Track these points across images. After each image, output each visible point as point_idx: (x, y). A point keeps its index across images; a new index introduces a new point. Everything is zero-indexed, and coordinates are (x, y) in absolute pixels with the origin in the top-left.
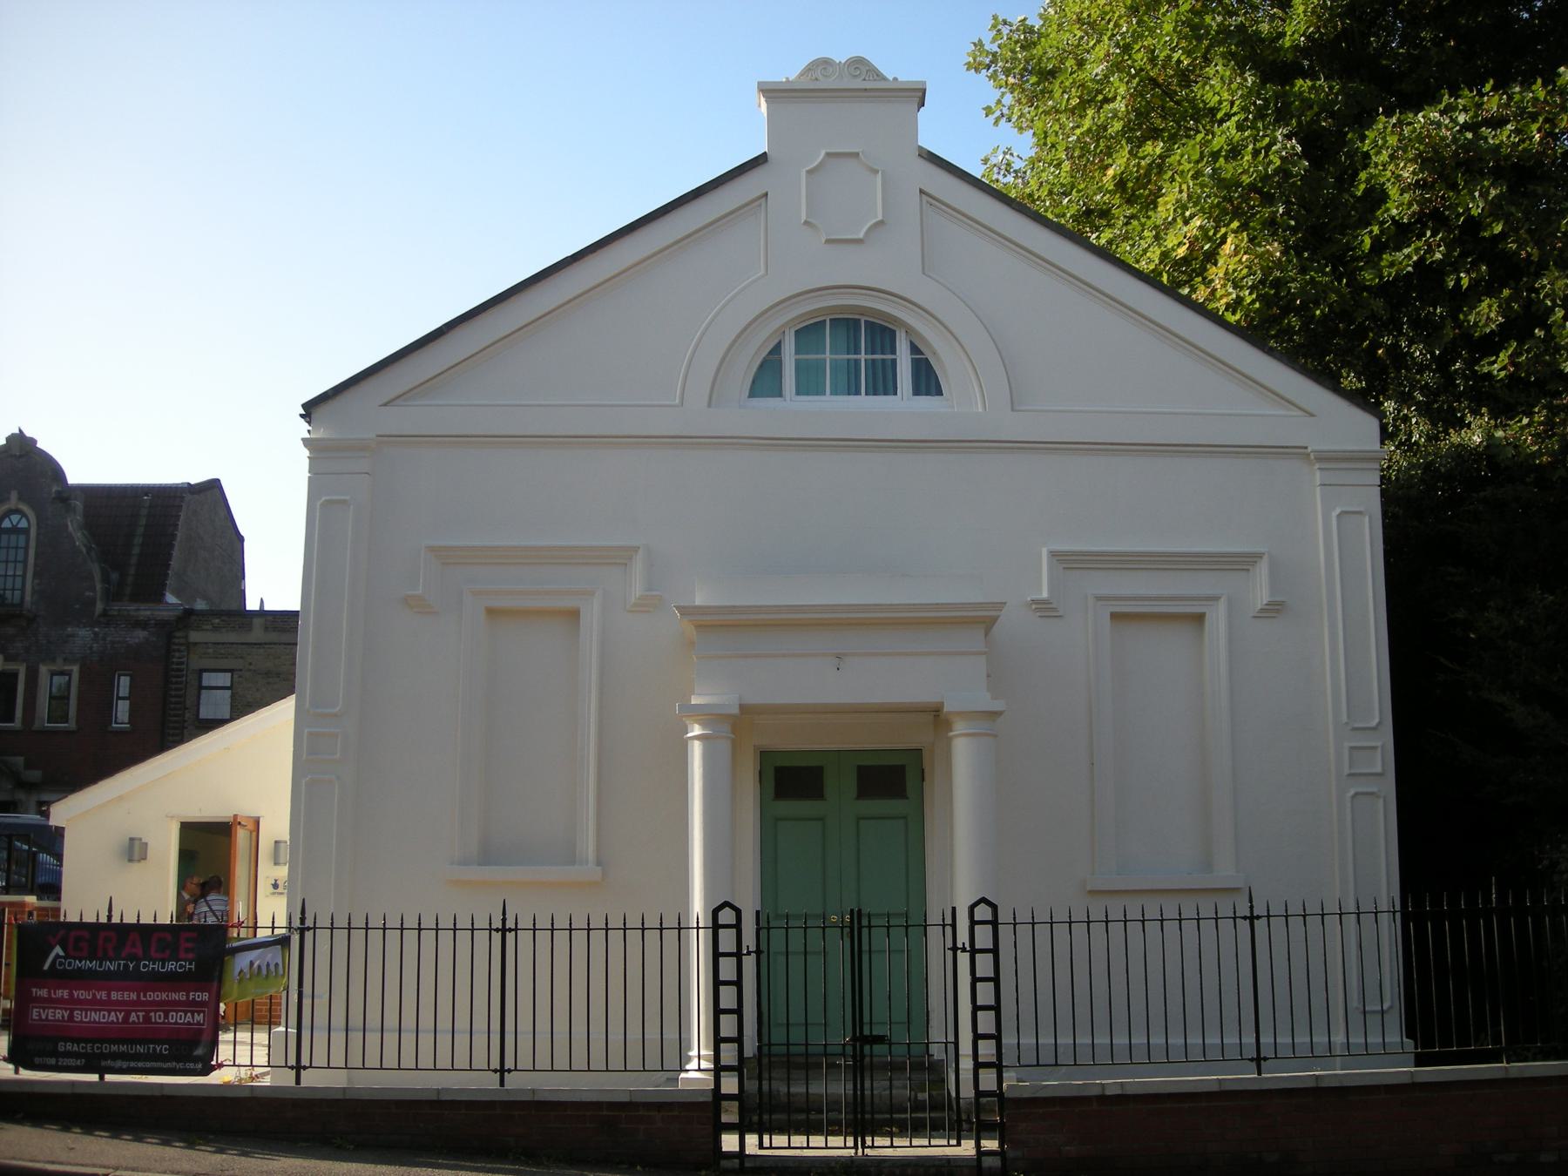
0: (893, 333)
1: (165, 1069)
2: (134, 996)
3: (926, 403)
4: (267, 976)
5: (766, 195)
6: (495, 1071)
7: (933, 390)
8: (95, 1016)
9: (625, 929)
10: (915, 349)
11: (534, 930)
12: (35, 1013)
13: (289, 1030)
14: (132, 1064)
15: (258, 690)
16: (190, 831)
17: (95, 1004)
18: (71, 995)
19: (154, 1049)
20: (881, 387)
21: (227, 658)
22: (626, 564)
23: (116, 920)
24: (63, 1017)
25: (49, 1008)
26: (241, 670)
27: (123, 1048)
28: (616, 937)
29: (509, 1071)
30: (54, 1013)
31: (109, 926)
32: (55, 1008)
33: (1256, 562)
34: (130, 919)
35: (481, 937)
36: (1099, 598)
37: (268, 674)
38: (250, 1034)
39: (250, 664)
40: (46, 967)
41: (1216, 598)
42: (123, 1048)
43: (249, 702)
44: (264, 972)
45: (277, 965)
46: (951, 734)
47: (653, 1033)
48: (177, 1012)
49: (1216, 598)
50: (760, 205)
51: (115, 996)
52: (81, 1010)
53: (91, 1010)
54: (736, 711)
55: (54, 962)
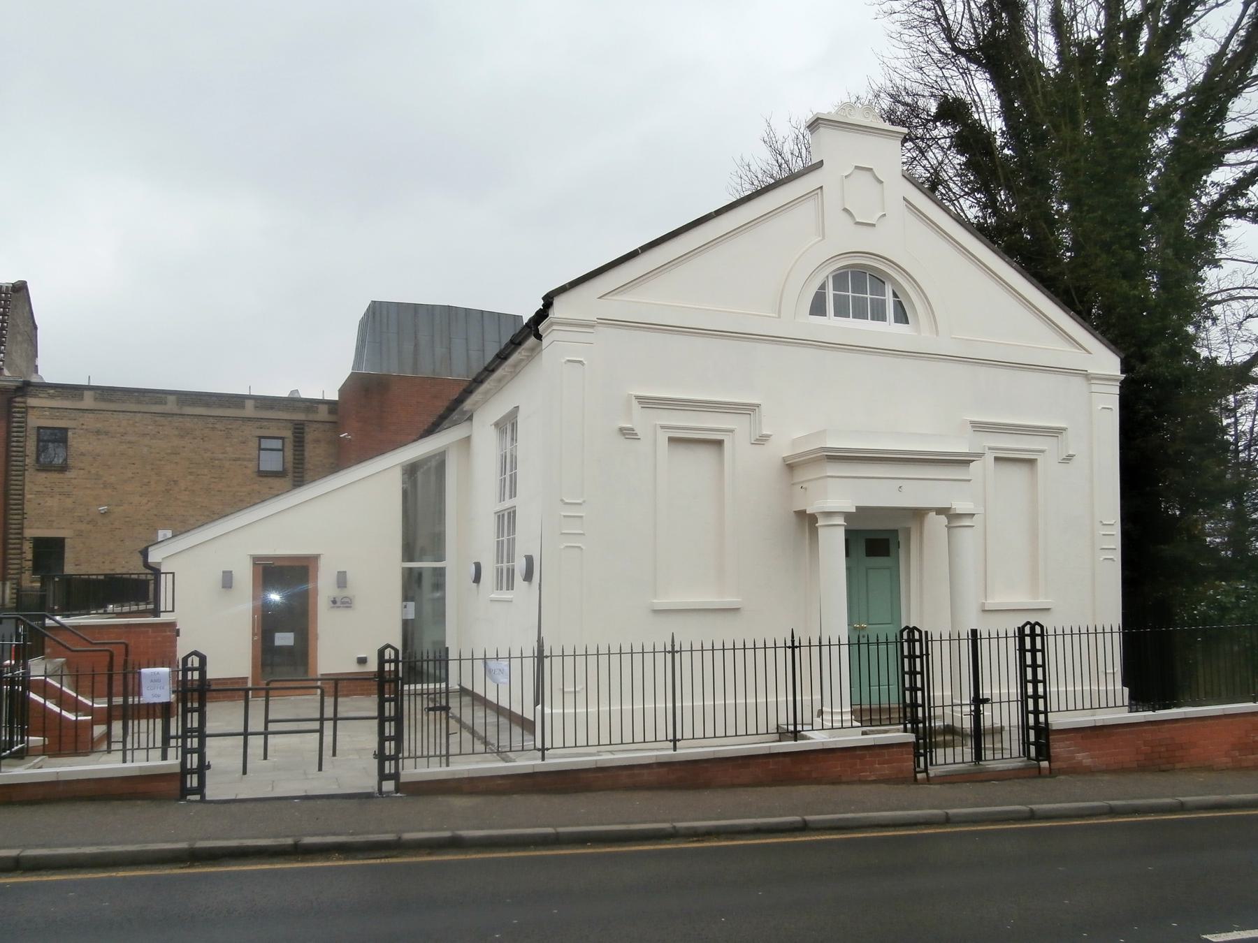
3: (901, 328)
5: (821, 187)
6: (670, 741)
7: (904, 321)
9: (775, 648)
10: (895, 295)
11: (830, 645)
15: (90, 444)
20: (876, 318)
21: (62, 419)
26: (74, 429)
28: (697, 655)
29: (548, 749)
35: (781, 652)
36: (662, 427)
37: (98, 432)
39: (83, 424)
43: (82, 452)
46: (817, 525)
50: (817, 194)
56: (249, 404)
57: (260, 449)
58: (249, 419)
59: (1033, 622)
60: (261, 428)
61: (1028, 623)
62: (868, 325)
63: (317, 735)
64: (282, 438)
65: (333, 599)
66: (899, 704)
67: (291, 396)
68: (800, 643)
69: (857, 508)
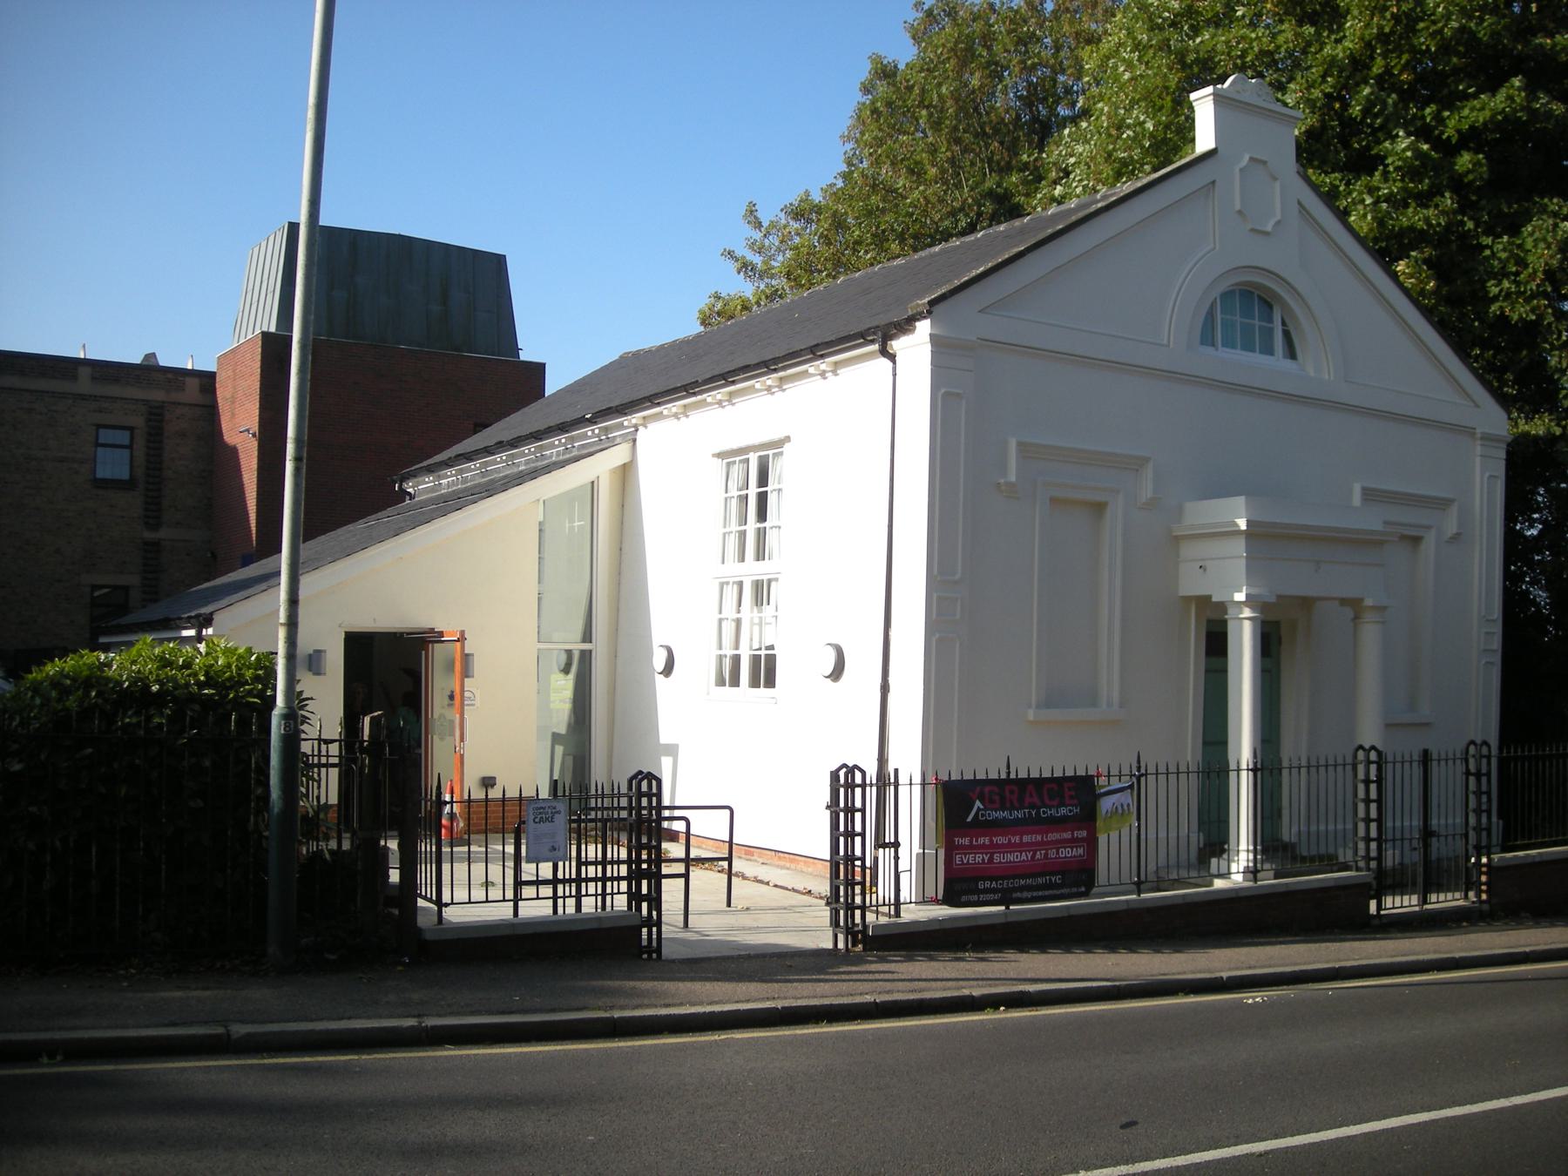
0: (1270, 307)
1: (1058, 895)
2: (1039, 838)
3: (1289, 364)
4: (1122, 814)
5: (1213, 182)
8: (1011, 857)
10: (1284, 323)
12: (957, 859)
13: (926, 851)
14: (1035, 894)
16: (360, 646)
17: (1011, 847)
18: (991, 841)
19: (1050, 880)
22: (1137, 470)
23: (1013, 776)
24: (983, 859)
25: (970, 853)
27: (1029, 881)
30: (975, 857)
31: (1008, 781)
32: (975, 853)
33: (1444, 510)
34: (1023, 775)
38: (450, 865)
40: (969, 819)
41: (1429, 527)
42: (1029, 881)
44: (1120, 811)
45: (1128, 805)
47: (1162, 835)
48: (1065, 848)
49: (1429, 527)
51: (1026, 839)
52: (1000, 853)
53: (1007, 852)
54: (1273, 599)
55: (977, 813)
56: (84, 372)
57: (98, 445)
58: (83, 397)
59: (850, 765)
60: (101, 412)
61: (844, 766)
62: (1258, 358)
63: (682, 880)
64: (131, 429)
65: (449, 694)
66: (596, 908)
67: (144, 363)
68: (1146, 770)
69: (1279, 597)
